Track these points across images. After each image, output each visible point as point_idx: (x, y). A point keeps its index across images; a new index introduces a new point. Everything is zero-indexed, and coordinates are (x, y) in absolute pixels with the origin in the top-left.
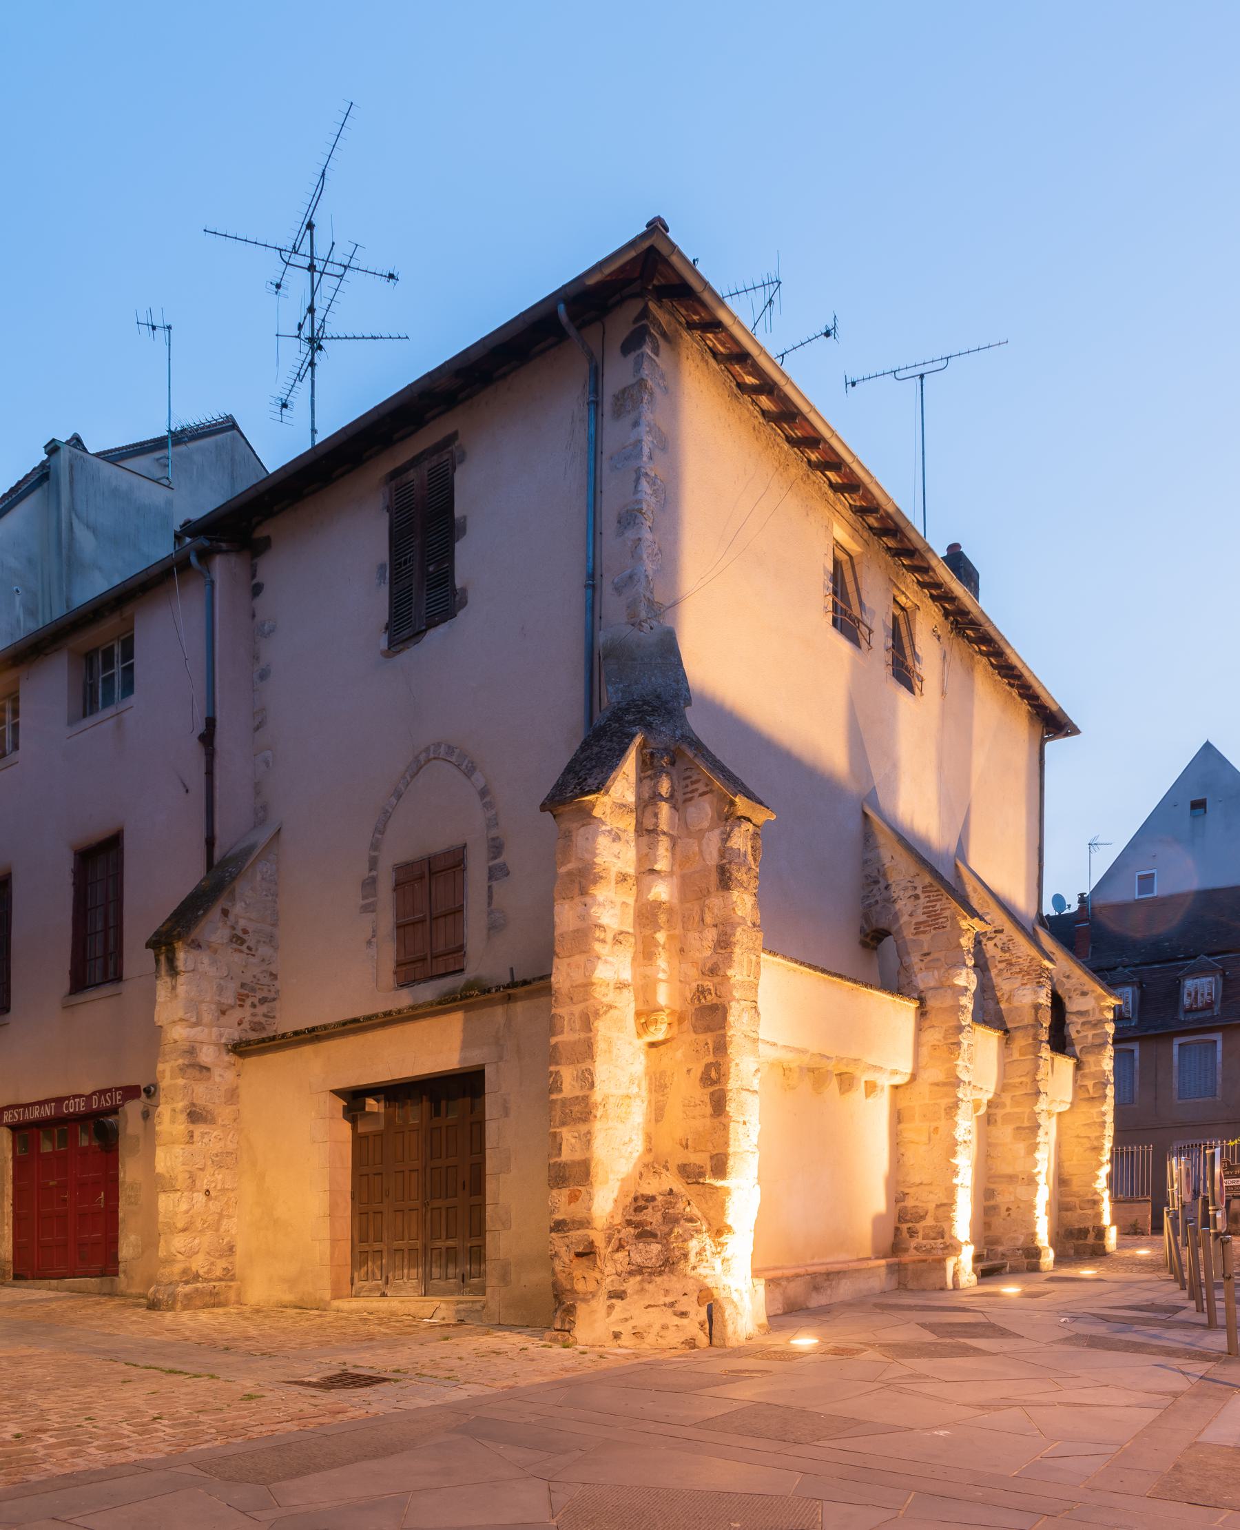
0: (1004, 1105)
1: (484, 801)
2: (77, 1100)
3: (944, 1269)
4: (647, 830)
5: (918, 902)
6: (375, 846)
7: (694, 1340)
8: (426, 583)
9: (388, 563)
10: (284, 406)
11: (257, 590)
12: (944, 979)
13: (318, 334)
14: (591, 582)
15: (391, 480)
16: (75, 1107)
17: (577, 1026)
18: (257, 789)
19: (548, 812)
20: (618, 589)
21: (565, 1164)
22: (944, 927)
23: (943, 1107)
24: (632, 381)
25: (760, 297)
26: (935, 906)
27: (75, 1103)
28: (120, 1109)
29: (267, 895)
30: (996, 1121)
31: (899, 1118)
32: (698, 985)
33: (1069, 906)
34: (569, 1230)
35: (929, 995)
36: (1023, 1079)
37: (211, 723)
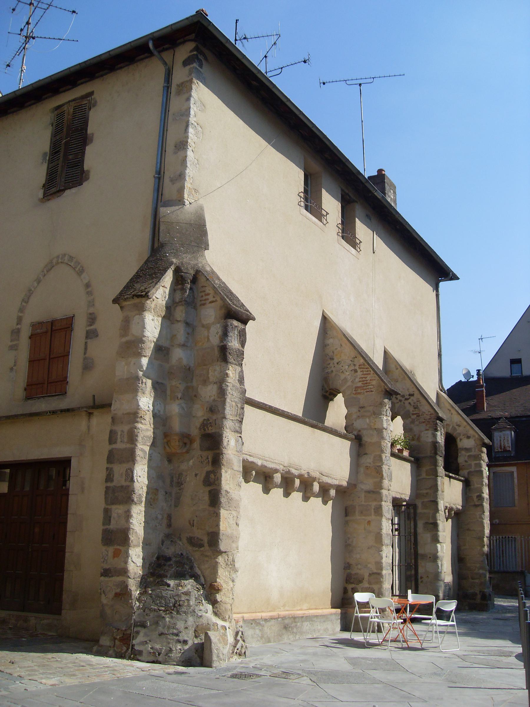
5: (356, 374)
6: (22, 310)
9: (49, 152)
10: (8, 66)
12: (372, 424)
13: (30, 34)
15: (56, 110)
17: (126, 440)
20: (173, 181)
22: (371, 391)
24: (188, 79)
25: (268, 42)
26: (366, 378)
33: (473, 376)
34: (112, 576)
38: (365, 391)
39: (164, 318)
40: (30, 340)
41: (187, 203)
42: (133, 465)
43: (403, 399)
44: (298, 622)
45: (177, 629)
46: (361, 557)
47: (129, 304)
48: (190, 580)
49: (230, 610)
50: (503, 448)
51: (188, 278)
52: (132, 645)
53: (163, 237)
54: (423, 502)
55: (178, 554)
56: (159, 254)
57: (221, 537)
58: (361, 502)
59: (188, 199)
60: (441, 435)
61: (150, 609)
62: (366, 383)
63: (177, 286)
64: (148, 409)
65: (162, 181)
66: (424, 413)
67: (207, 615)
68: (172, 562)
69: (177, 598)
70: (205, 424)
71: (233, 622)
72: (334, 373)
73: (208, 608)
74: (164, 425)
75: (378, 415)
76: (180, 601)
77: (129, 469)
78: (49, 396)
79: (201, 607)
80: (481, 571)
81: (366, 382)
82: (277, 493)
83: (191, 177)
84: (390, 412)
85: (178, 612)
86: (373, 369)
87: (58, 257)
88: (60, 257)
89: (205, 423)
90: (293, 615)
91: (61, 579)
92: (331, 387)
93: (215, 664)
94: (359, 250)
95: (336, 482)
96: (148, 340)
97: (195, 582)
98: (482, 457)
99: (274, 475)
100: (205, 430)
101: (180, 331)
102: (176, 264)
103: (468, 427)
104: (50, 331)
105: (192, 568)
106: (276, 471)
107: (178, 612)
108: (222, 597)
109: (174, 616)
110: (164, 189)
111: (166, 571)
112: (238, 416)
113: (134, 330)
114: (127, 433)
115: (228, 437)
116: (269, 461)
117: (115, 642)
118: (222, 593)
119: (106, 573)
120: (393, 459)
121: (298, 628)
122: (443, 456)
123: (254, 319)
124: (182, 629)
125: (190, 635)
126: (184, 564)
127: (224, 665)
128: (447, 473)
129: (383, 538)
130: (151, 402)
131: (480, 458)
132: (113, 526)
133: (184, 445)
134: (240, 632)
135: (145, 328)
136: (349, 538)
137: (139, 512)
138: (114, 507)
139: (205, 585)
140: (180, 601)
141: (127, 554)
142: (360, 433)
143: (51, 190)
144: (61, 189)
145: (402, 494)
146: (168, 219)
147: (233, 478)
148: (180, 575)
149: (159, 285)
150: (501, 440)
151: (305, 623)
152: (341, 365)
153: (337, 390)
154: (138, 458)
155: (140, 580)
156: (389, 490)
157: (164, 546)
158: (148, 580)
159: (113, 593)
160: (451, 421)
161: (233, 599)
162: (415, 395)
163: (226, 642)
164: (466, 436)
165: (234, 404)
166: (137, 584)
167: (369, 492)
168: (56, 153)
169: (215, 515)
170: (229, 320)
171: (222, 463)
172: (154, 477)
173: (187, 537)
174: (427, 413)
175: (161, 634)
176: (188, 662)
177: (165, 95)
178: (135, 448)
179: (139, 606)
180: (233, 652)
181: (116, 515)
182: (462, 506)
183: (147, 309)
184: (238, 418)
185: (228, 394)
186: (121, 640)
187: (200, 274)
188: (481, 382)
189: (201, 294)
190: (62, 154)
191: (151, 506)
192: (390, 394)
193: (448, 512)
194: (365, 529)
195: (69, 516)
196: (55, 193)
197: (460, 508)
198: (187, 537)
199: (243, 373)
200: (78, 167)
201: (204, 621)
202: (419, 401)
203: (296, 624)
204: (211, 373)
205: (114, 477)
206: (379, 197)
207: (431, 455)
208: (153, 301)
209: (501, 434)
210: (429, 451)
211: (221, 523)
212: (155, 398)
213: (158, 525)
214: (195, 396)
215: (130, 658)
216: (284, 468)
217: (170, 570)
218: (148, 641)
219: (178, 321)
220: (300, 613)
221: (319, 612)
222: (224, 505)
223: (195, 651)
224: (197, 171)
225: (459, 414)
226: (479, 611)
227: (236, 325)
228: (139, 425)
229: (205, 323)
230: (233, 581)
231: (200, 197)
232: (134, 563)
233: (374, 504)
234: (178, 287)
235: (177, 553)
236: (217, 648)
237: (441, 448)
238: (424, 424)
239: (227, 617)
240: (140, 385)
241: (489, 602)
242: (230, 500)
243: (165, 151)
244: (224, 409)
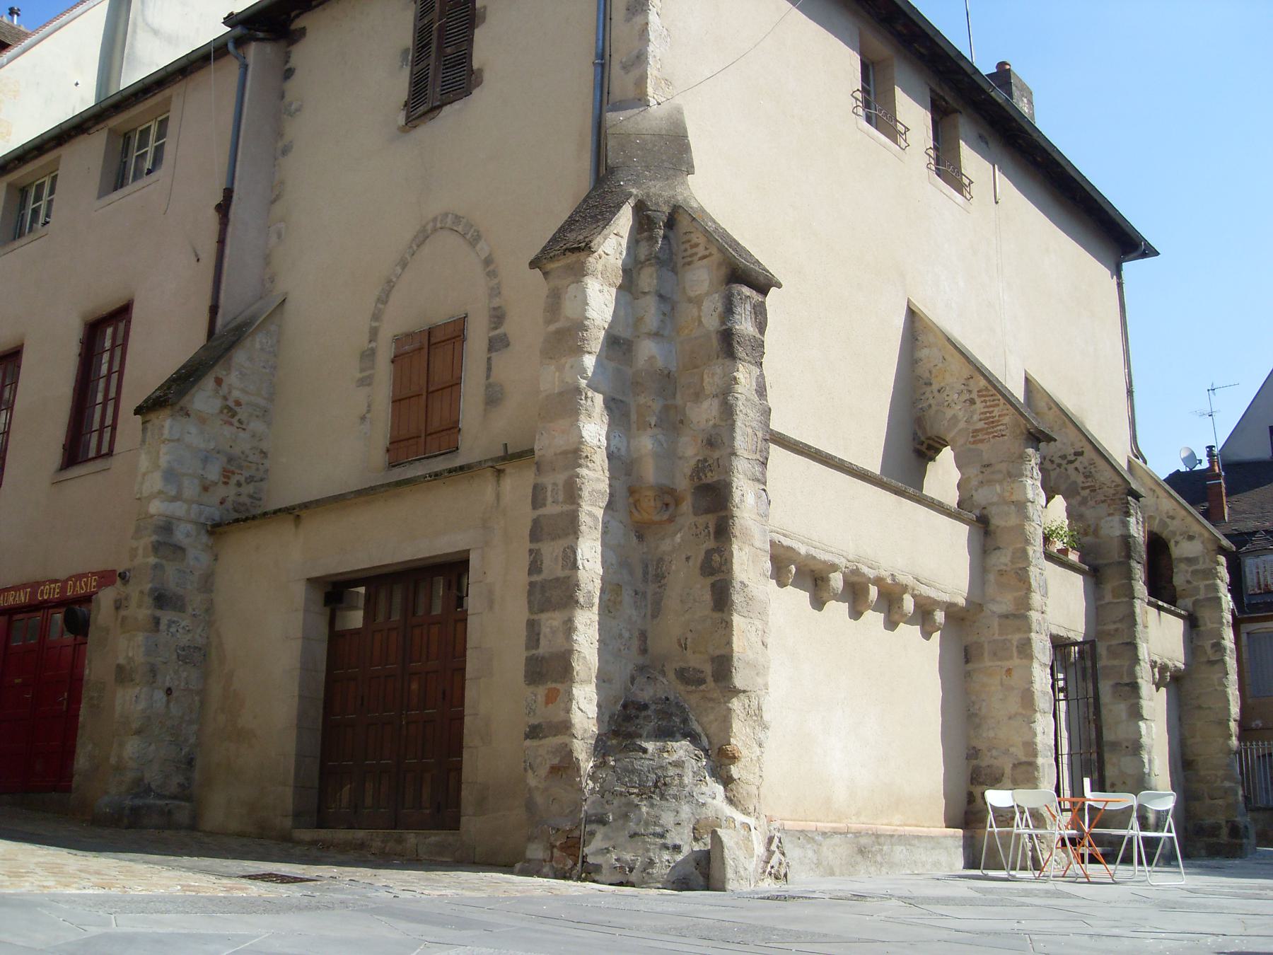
1: (488, 270)
2: (53, 586)
5: (974, 407)
6: (376, 317)
9: (411, 48)
11: (288, 74)
12: (1007, 494)
16: (50, 593)
17: (561, 498)
18: (267, 259)
20: (626, 68)
21: (543, 658)
22: (1002, 435)
26: (993, 412)
27: (50, 589)
28: (94, 597)
29: (264, 367)
31: (966, 656)
33: (1200, 462)
34: (545, 737)
36: (1118, 625)
37: (228, 193)
38: (991, 436)
39: (620, 288)
40: (392, 366)
41: (652, 102)
42: (575, 540)
43: (1064, 462)
44: (884, 844)
45: (662, 826)
46: (996, 735)
47: (558, 267)
48: (683, 742)
49: (757, 796)
50: (1262, 586)
51: (660, 218)
52: (583, 857)
53: (613, 158)
54: (1109, 648)
55: (660, 699)
56: (606, 184)
57: (735, 663)
58: (994, 635)
59: (655, 96)
60: (1138, 523)
61: (613, 793)
62: (991, 423)
63: (641, 233)
64: (598, 444)
67: (715, 801)
68: (649, 712)
69: (659, 772)
70: (701, 468)
71: (764, 820)
72: (934, 408)
73: (716, 790)
74: (628, 474)
75: (1015, 477)
76: (665, 777)
77: (568, 548)
78: (428, 458)
79: (704, 789)
80: (1227, 784)
81: (992, 420)
82: (838, 610)
84: (1039, 473)
85: (662, 797)
86: (1004, 396)
87: (435, 220)
89: (700, 466)
90: (874, 830)
91: (458, 769)
92: (929, 435)
93: (730, 885)
94: (968, 196)
95: (946, 598)
96: (594, 325)
97: (691, 745)
98: (1217, 573)
99: (831, 575)
100: (700, 479)
101: (650, 311)
102: (637, 195)
103: (1189, 519)
104: (426, 346)
105: (685, 721)
106: (834, 567)
107: (662, 797)
108: (742, 771)
109: (655, 803)
110: (611, 83)
111: (639, 726)
112: (758, 453)
113: (569, 309)
114: (564, 487)
115: (741, 488)
116: (819, 549)
117: (552, 853)
118: (740, 764)
119: (534, 732)
120: (1049, 565)
121: (885, 855)
123: (779, 285)
124: (670, 826)
125: (685, 837)
126: (671, 715)
127: (746, 887)
128: (1153, 599)
129: (1036, 698)
130: (604, 433)
131: (1215, 575)
132: (544, 649)
133: (664, 506)
134: (776, 837)
135: (587, 304)
136: (973, 703)
137: (589, 622)
138: (543, 616)
139: (709, 751)
140: (665, 777)
141: (569, 695)
142: (985, 512)
143: (418, 110)
144: (434, 105)
145: (1069, 630)
146: (621, 129)
147: (753, 562)
148: (665, 734)
149: (608, 230)
150: (1258, 573)
151: (898, 847)
153: (941, 439)
154: (583, 528)
155: (594, 742)
156: (1043, 613)
157: (635, 686)
158: (609, 743)
159: (548, 766)
160: (1157, 509)
161: (761, 776)
162: (1085, 454)
163: (750, 852)
164: (1186, 537)
165: (750, 431)
166: (590, 749)
167: (1006, 617)
168: (423, 47)
169: (724, 625)
170: (734, 285)
171: (732, 533)
172: (613, 562)
173: (676, 670)
174: (1109, 485)
175: (634, 835)
176: (682, 883)
178: (578, 510)
179: (594, 787)
180: (764, 872)
181: (548, 630)
182: (1184, 664)
183: (590, 272)
184: (759, 457)
185: (738, 412)
186: (564, 848)
187: (681, 211)
188: (1216, 468)
189: (683, 247)
190: (434, 46)
191: (610, 614)
192: (1036, 438)
193: (1159, 672)
194: (1002, 685)
195: (469, 653)
196: (425, 114)
197: (1183, 667)
198: (676, 670)
199: (764, 378)
200: (463, 65)
201: (709, 813)
202: (1094, 463)
203: (881, 847)
204: (707, 379)
205: (544, 565)
206: (1000, 101)
207: (1121, 560)
208: (600, 258)
209: (1260, 560)
210: (1115, 554)
211: (735, 639)
212: (609, 425)
213: (622, 648)
214: (682, 422)
215: (580, 879)
217: (648, 725)
218: (610, 848)
219: (645, 293)
220: (887, 829)
221: (924, 831)
222: (739, 608)
223: (694, 864)
224: (667, 48)
225: (1171, 496)
226: (1228, 858)
227: (748, 294)
228: (583, 471)
229: (692, 294)
230: (760, 746)
231: (675, 93)
232: (582, 711)
233: (1016, 638)
234: (642, 235)
235: (658, 696)
236: (734, 856)
237: (1139, 547)
238: (1104, 506)
239: (752, 809)
240: (583, 402)
241: (1245, 841)
242: (749, 599)
243: (611, 19)
244: (733, 439)
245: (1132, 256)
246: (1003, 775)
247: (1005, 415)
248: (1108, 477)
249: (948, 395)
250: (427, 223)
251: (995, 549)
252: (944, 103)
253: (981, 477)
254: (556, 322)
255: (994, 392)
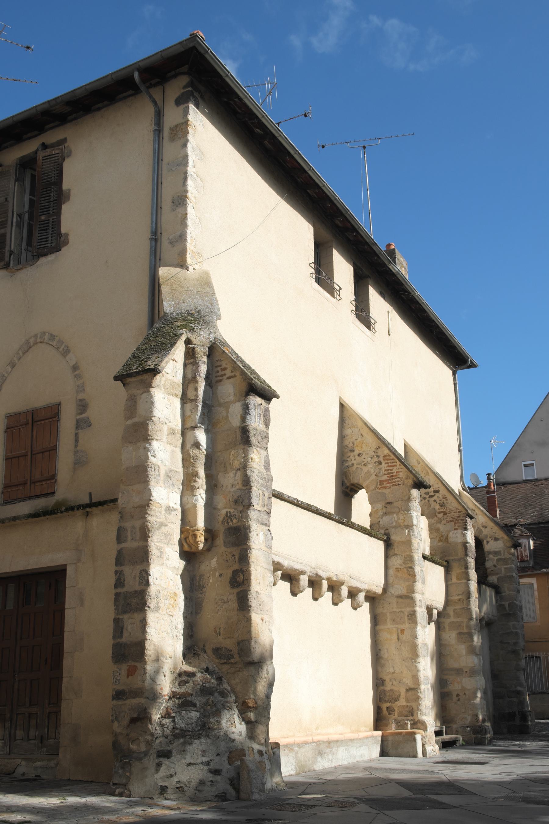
0: (449, 616)
3: (415, 740)
4: (190, 399)
7: (225, 793)
8: (38, 226)
12: (401, 521)
14: (154, 237)
19: (119, 382)
20: (172, 243)
22: (399, 485)
23: (407, 614)
24: (183, 121)
30: (444, 628)
32: (227, 512)
34: (127, 699)
35: (392, 532)
38: (391, 485)
43: (427, 496)
44: (333, 747)
50: (520, 557)
58: (392, 608)
62: (392, 477)
65: (159, 243)
66: (451, 511)
72: (355, 466)
77: (143, 571)
81: (391, 475)
83: (193, 238)
87: (36, 336)
88: (39, 336)
92: (352, 482)
104: (30, 422)
106: (303, 573)
112: (265, 506)
122: (474, 557)
123: (277, 397)
132: (125, 638)
138: (126, 616)
152: (363, 457)
167: (400, 597)
174: (454, 510)
177: (157, 142)
189: (216, 370)
199: (268, 458)
202: (446, 498)
216: (312, 569)
222: (256, 609)
238: (453, 523)
240: (153, 472)
245: (463, 367)
246: (399, 696)
247: (400, 472)
248: (454, 506)
249: (364, 458)
250: (30, 338)
251: (394, 555)
252: (360, 271)
253: (384, 510)
254: (133, 418)
255: (393, 457)
